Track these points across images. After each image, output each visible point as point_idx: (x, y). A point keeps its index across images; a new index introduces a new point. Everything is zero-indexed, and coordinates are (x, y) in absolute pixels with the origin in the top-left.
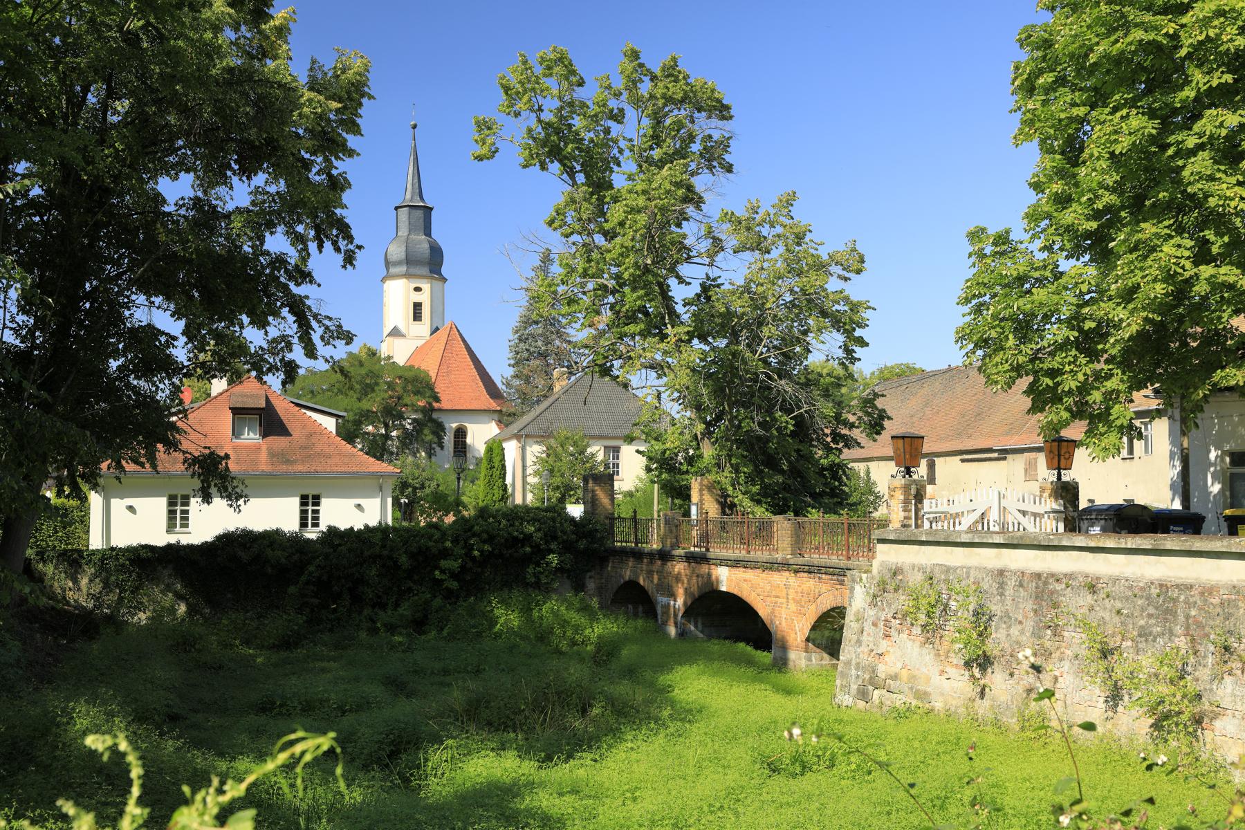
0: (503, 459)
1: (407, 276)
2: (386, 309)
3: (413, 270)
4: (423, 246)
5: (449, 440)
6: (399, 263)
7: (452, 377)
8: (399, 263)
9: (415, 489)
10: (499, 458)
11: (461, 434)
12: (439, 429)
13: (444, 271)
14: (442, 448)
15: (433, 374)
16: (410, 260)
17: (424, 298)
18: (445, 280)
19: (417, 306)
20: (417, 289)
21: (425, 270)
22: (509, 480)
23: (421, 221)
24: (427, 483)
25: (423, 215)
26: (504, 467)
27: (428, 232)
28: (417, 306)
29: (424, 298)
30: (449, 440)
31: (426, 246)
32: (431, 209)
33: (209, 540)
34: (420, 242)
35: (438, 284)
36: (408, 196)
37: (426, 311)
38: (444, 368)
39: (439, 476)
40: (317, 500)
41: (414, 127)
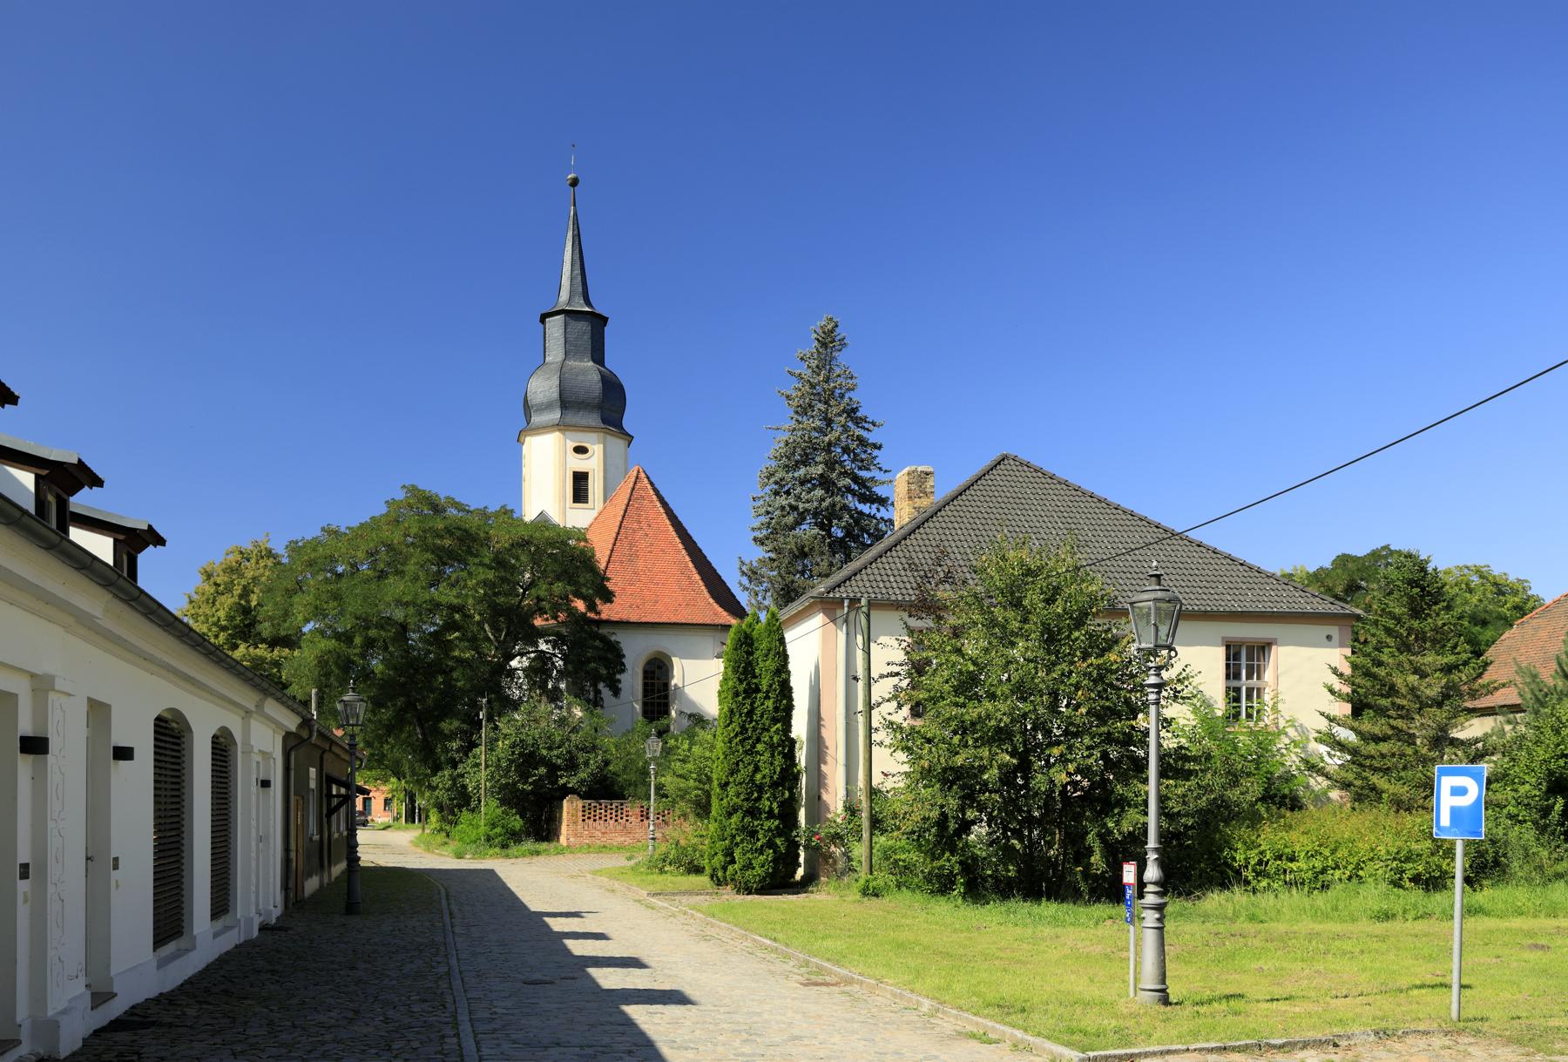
0: (782, 669)
1: (561, 426)
2: (526, 486)
3: (572, 418)
4: (587, 372)
5: (632, 681)
6: (548, 407)
7: (640, 564)
8: (548, 407)
9: (553, 769)
10: (771, 664)
11: (657, 674)
12: (613, 659)
13: (626, 424)
14: (616, 692)
15: (601, 558)
16: (568, 402)
17: (592, 464)
18: (629, 438)
19: (580, 480)
20: (580, 450)
21: (594, 419)
22: (799, 728)
23: (587, 337)
24: (582, 757)
25: (592, 328)
26: (786, 691)
27: (598, 356)
28: (580, 480)
29: (592, 464)
30: (632, 681)
31: (596, 377)
32: (605, 320)
33: (1328, 564)
34: (584, 371)
35: (618, 444)
36: (564, 295)
37: (595, 487)
38: (623, 547)
39: (607, 742)
40: (1261, 649)
41: (574, 183)
